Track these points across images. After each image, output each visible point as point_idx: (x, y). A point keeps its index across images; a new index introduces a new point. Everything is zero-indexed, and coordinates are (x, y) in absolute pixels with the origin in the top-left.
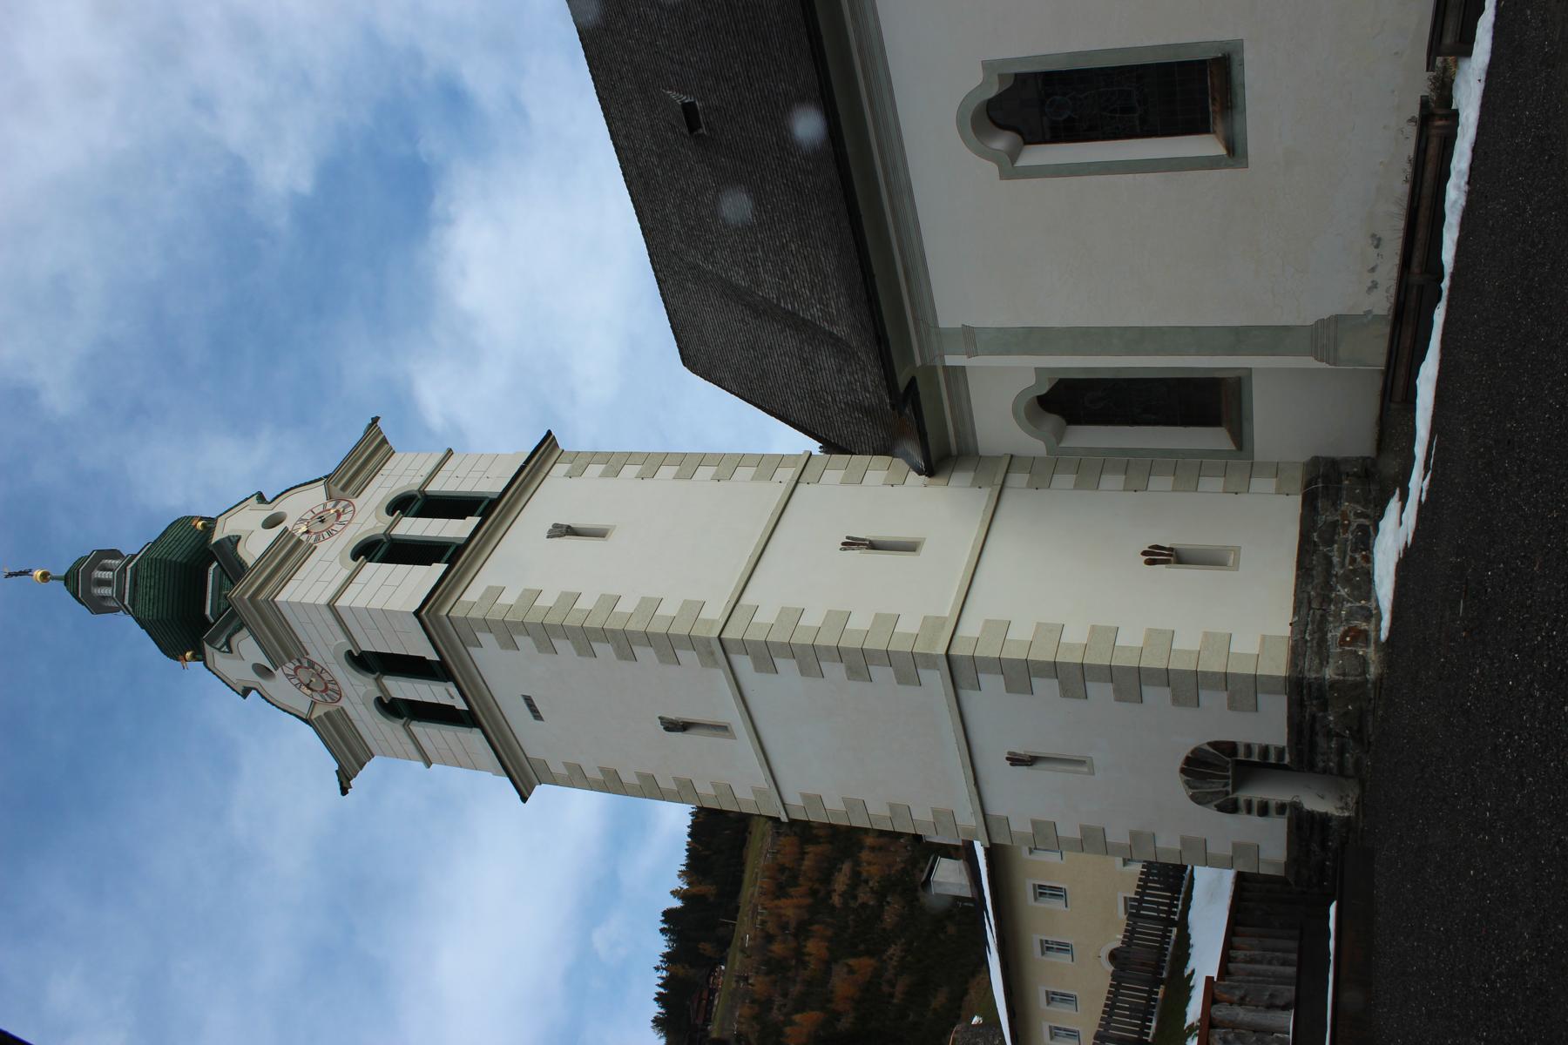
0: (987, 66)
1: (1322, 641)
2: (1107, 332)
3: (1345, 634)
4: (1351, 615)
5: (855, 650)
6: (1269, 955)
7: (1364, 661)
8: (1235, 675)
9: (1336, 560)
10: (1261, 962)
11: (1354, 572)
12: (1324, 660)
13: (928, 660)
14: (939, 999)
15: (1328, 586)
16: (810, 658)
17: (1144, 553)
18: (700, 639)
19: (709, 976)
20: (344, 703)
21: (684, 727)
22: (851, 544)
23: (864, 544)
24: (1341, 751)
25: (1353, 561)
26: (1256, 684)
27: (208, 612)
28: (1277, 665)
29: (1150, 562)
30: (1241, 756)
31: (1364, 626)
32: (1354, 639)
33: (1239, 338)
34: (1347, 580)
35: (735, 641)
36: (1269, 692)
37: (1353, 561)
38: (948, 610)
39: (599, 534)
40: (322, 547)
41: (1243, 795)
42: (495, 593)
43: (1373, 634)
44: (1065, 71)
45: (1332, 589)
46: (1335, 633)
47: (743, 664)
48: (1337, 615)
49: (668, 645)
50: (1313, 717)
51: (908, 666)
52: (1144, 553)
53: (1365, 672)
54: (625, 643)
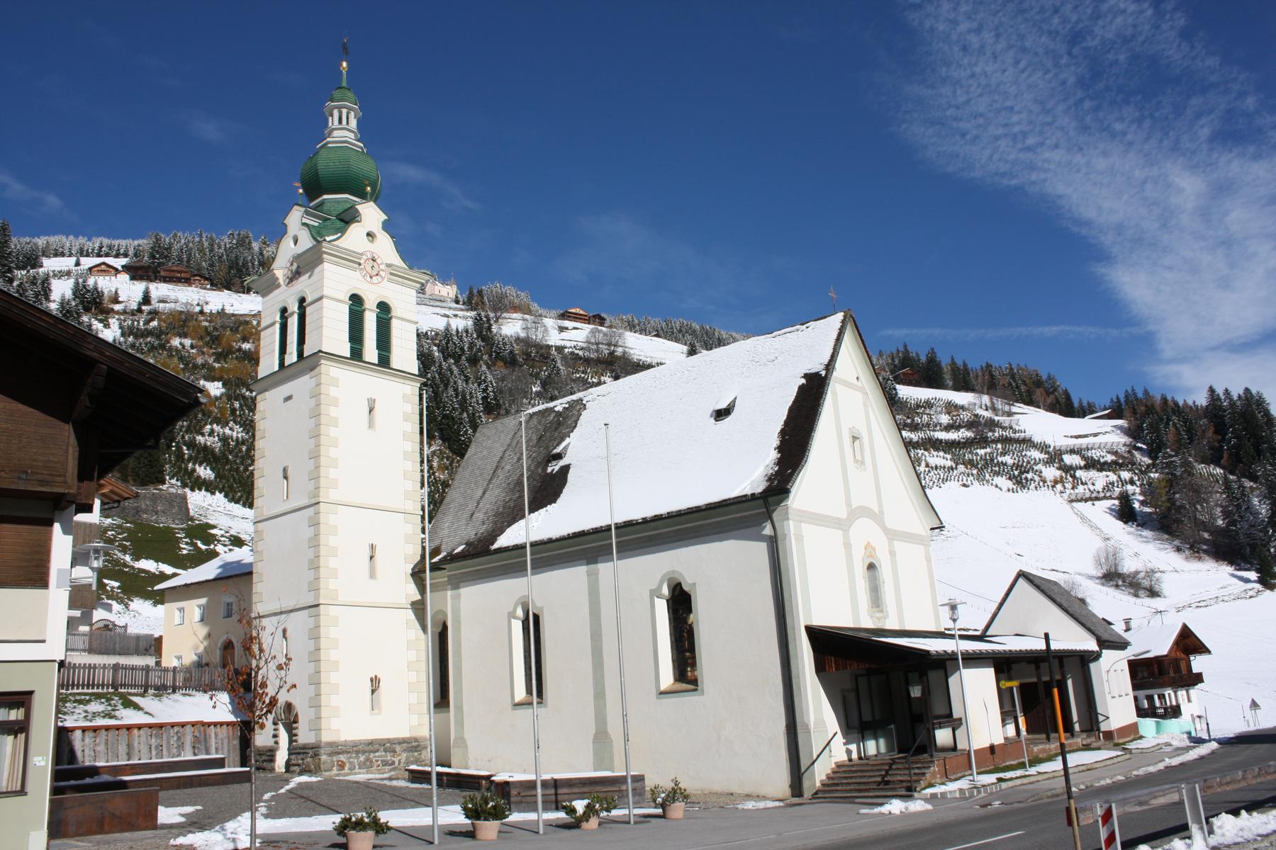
0: (542, 608)
1: (339, 753)
2: (200, 785)
3: (342, 762)
4: (350, 763)
5: (319, 563)
6: (220, 742)
7: (331, 770)
8: (321, 722)
9: (377, 754)
10: (216, 738)
11: (372, 762)
12: (330, 755)
13: (317, 596)
14: (205, 472)
15: (364, 752)
16: (315, 542)
17: (376, 677)
18: (319, 492)
19: (201, 276)
20: (283, 287)
21: (286, 477)
22: (372, 547)
23: (585, 319)
24: (298, 765)
25: (377, 761)
26: (318, 730)
27: (325, 197)
28: (326, 737)
29: (372, 680)
30: (294, 725)
31: (346, 768)
32: (340, 765)
33: (460, 708)
34: (367, 759)
35: (319, 509)
36: (316, 734)
37: (377, 761)
38: (341, 599)
39: (371, 425)
40: (357, 275)
41: (281, 727)
42: (335, 382)
43: (342, 772)
44: (1055, 413)
45: (363, 754)
46: (342, 758)
47: (310, 511)
48: (351, 757)
49: (315, 477)
50: (308, 753)
51: (314, 587)
52: (376, 677)
53: (325, 771)
54: (315, 456)
